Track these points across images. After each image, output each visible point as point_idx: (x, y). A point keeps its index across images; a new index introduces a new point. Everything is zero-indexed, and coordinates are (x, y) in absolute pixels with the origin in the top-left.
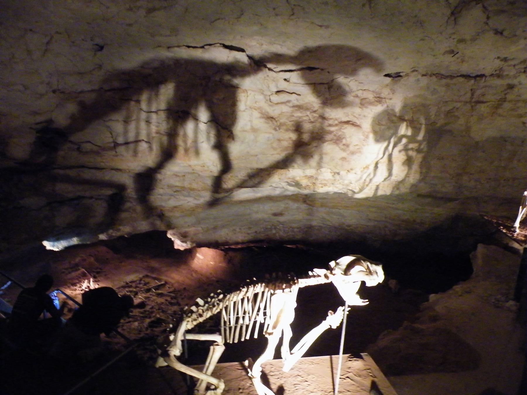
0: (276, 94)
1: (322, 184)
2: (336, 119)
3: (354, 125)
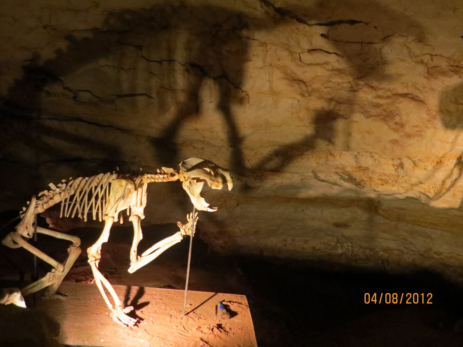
0: (308, 52)
1: (381, 180)
3: (414, 99)
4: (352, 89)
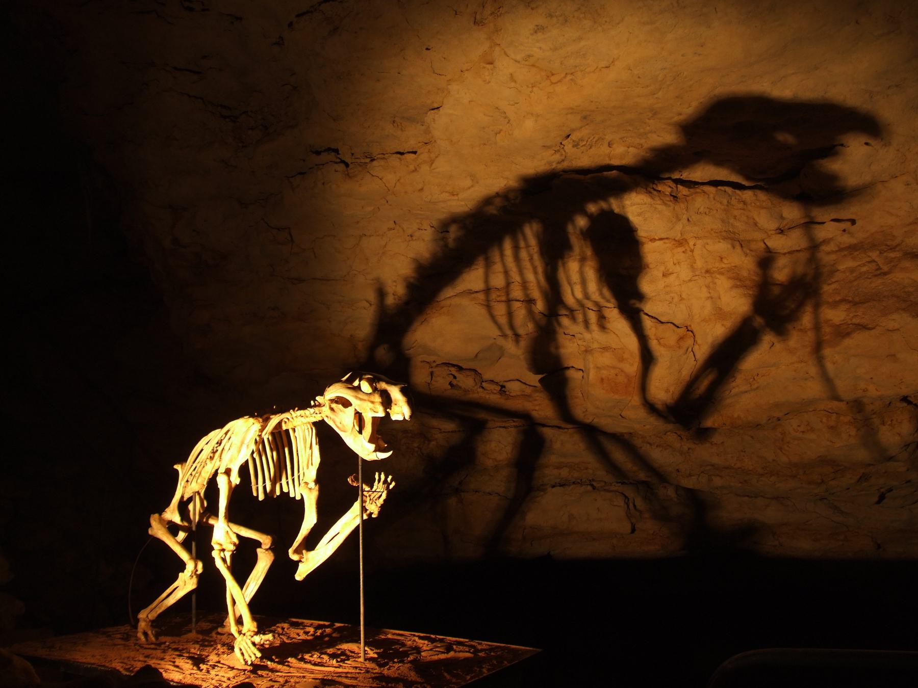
4: (879, 272)
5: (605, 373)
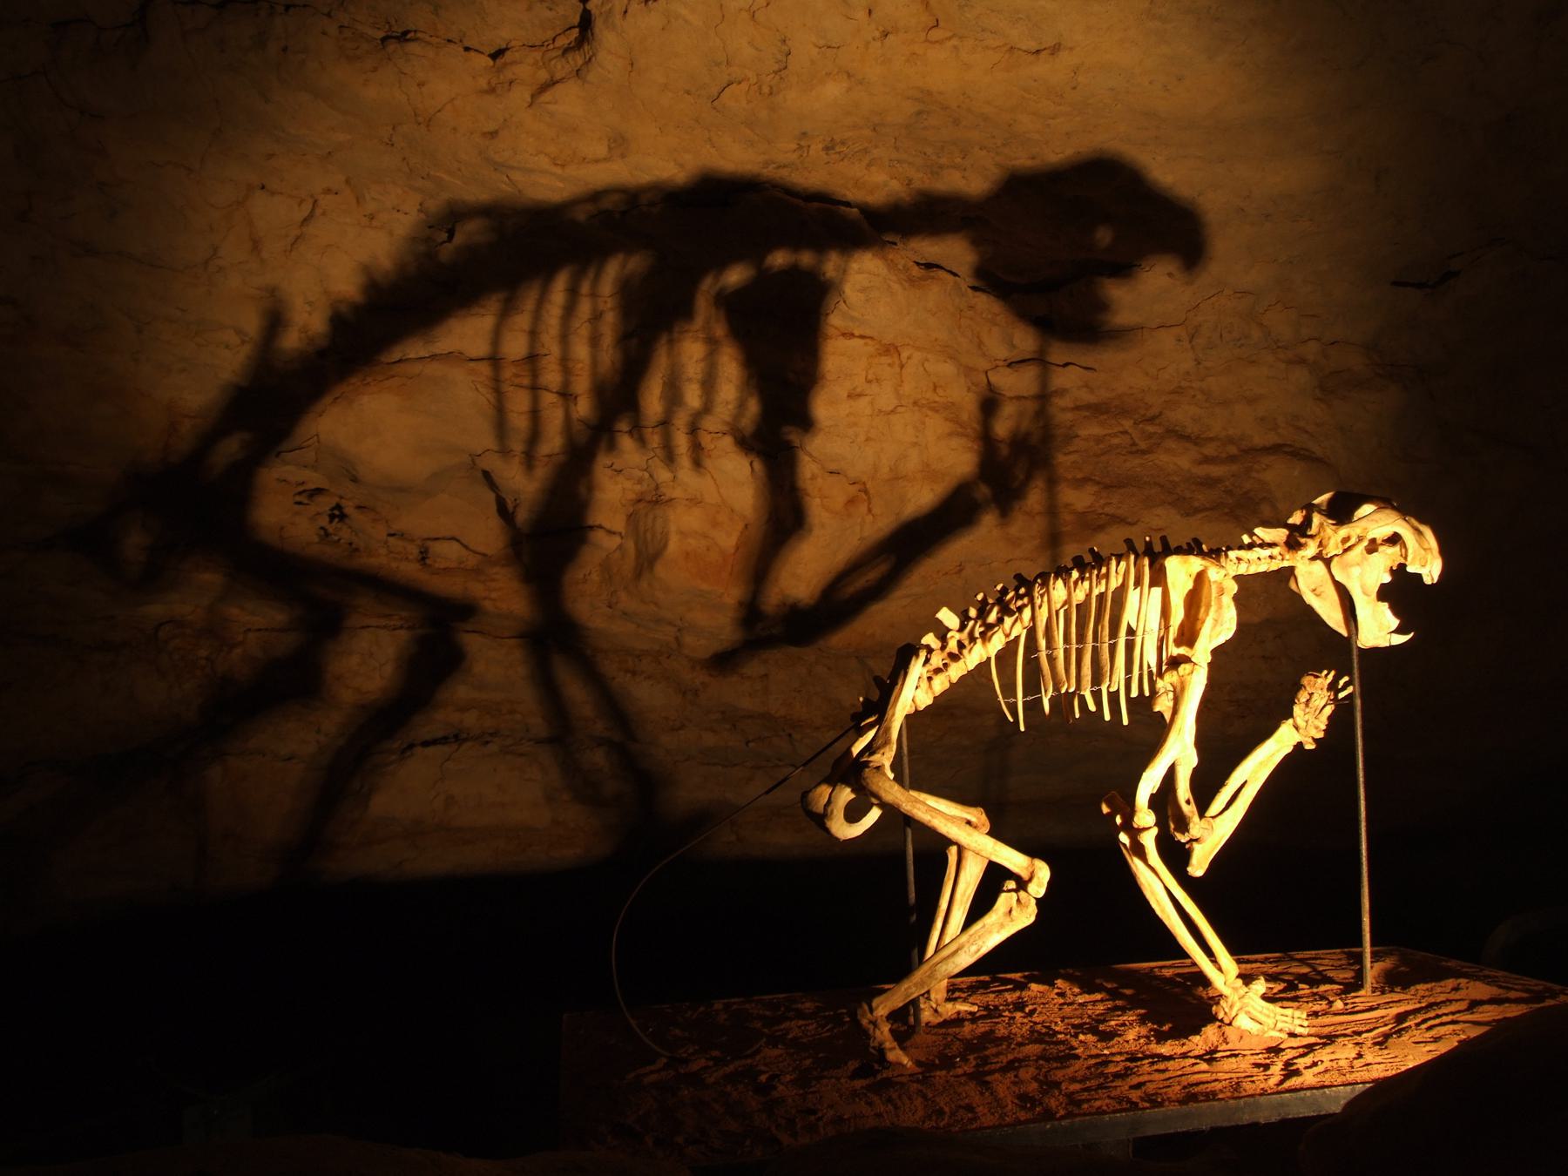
2: (1231, 441)
5: (692, 543)
